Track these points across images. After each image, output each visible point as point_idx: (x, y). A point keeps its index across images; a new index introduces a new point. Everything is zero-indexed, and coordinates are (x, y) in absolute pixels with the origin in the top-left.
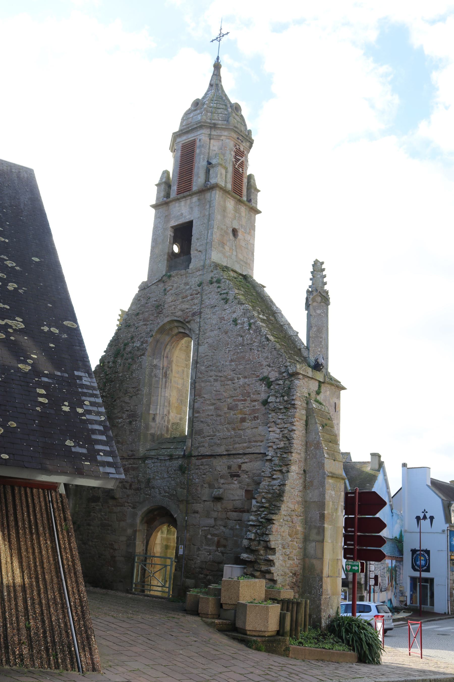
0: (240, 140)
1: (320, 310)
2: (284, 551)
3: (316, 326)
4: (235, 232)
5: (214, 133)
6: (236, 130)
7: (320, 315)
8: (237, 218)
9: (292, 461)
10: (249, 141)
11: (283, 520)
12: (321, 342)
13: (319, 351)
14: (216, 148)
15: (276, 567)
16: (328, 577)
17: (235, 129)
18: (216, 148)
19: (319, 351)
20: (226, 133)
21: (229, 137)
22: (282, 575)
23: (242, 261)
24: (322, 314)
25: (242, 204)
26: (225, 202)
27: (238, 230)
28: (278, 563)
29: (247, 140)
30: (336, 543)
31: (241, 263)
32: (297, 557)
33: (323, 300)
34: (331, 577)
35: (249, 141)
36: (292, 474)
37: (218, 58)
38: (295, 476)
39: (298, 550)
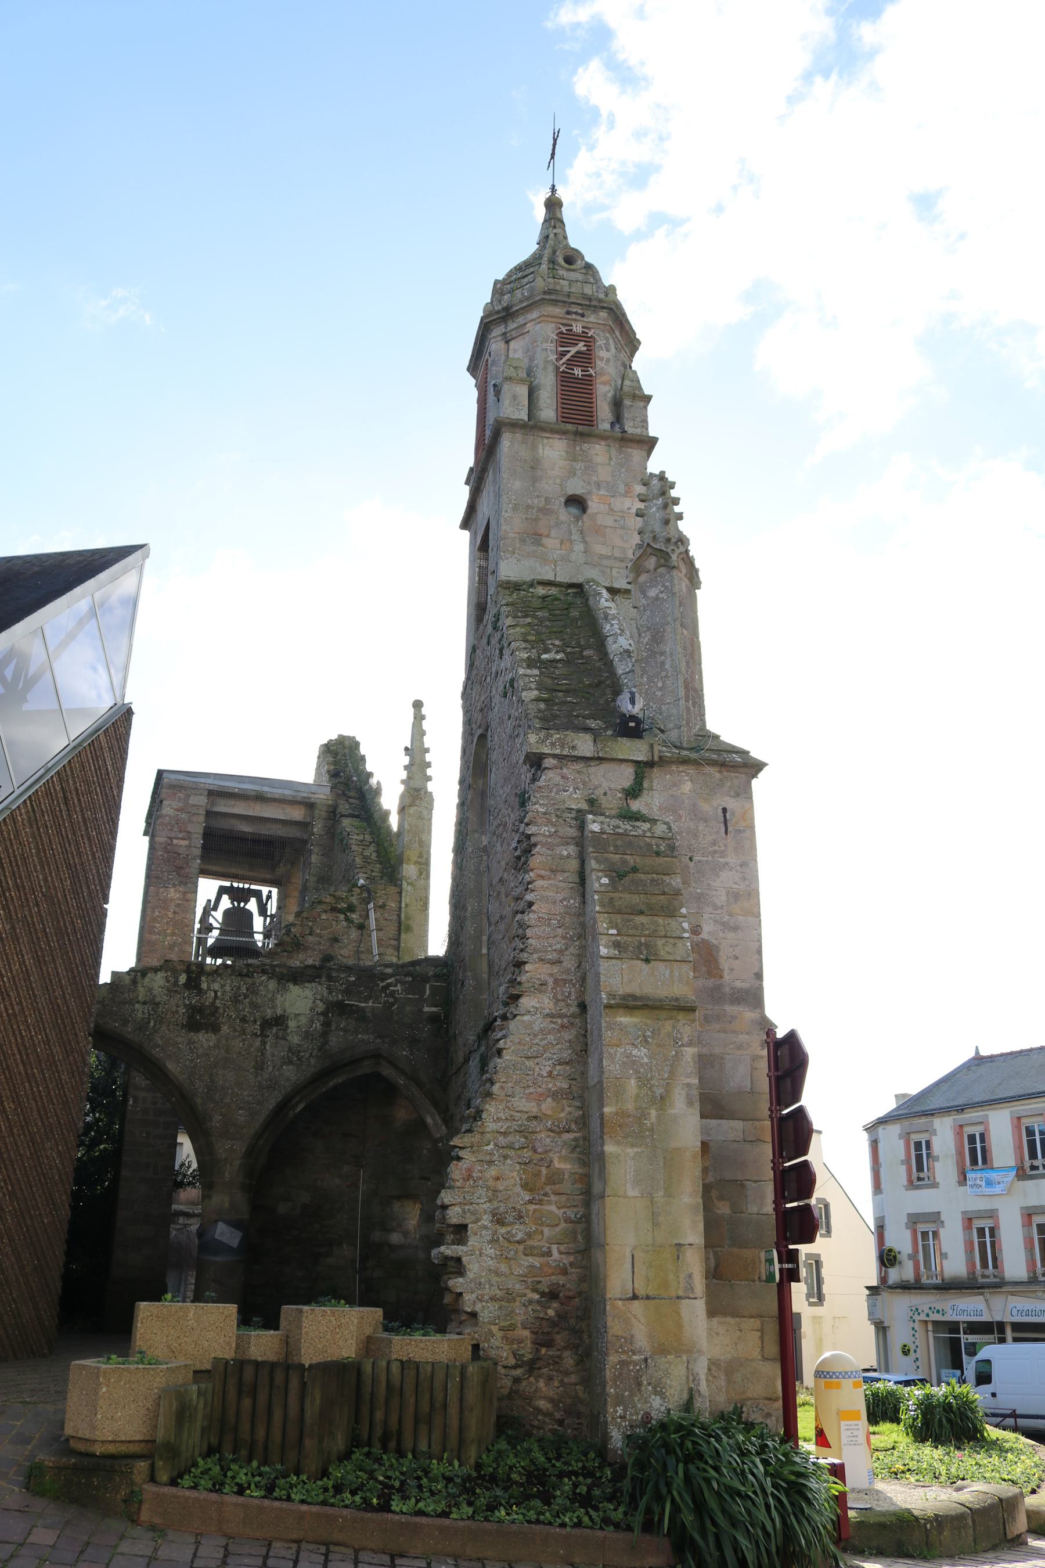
0: (576, 313)
1: (656, 587)
2: (503, 1230)
3: (649, 629)
4: (577, 502)
5: (512, 325)
6: (553, 297)
7: (657, 598)
8: (578, 472)
9: (526, 985)
10: (603, 308)
11: (496, 1145)
12: (663, 663)
13: (660, 689)
14: (519, 355)
15: (470, 1275)
16: (635, 1297)
17: (547, 297)
18: (519, 355)
19: (660, 689)
20: (534, 315)
21: (538, 321)
22: (493, 1299)
23: (608, 558)
24: (661, 596)
25: (593, 440)
26: (534, 448)
27: (587, 497)
28: (473, 1268)
29: (595, 307)
30: (669, 1195)
31: (605, 562)
32: (562, 1248)
33: (662, 561)
34: (648, 1298)
35: (603, 308)
36: (526, 1018)
37: (553, 189)
38: (539, 1023)
39: (563, 1225)
